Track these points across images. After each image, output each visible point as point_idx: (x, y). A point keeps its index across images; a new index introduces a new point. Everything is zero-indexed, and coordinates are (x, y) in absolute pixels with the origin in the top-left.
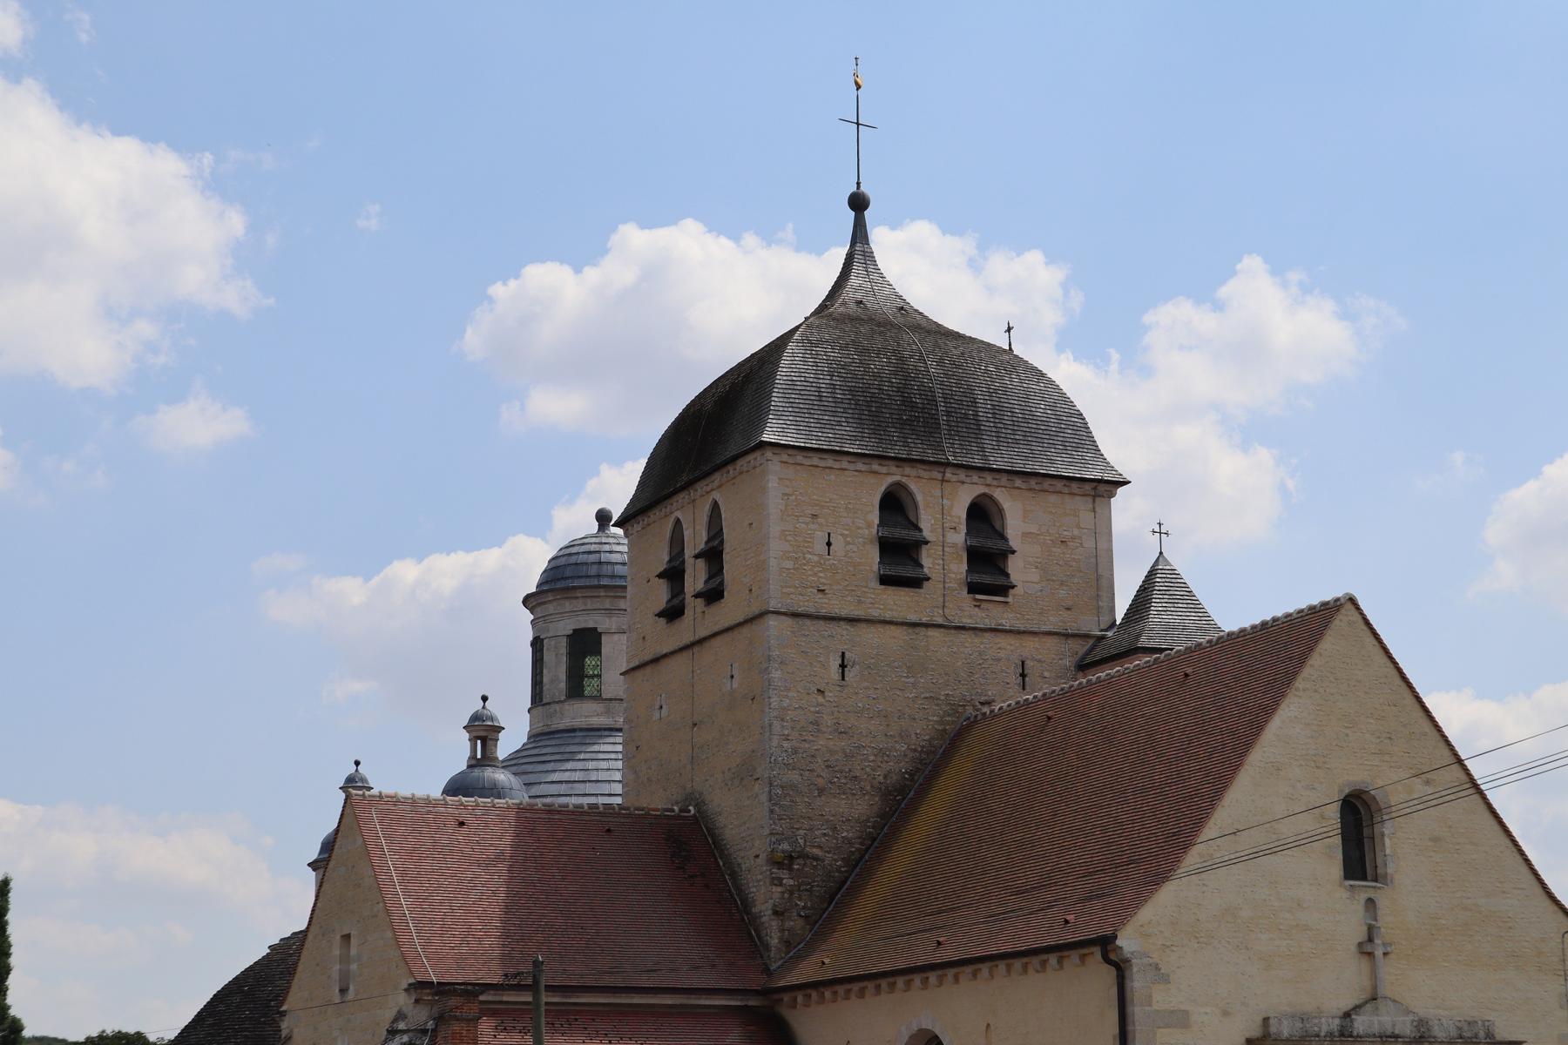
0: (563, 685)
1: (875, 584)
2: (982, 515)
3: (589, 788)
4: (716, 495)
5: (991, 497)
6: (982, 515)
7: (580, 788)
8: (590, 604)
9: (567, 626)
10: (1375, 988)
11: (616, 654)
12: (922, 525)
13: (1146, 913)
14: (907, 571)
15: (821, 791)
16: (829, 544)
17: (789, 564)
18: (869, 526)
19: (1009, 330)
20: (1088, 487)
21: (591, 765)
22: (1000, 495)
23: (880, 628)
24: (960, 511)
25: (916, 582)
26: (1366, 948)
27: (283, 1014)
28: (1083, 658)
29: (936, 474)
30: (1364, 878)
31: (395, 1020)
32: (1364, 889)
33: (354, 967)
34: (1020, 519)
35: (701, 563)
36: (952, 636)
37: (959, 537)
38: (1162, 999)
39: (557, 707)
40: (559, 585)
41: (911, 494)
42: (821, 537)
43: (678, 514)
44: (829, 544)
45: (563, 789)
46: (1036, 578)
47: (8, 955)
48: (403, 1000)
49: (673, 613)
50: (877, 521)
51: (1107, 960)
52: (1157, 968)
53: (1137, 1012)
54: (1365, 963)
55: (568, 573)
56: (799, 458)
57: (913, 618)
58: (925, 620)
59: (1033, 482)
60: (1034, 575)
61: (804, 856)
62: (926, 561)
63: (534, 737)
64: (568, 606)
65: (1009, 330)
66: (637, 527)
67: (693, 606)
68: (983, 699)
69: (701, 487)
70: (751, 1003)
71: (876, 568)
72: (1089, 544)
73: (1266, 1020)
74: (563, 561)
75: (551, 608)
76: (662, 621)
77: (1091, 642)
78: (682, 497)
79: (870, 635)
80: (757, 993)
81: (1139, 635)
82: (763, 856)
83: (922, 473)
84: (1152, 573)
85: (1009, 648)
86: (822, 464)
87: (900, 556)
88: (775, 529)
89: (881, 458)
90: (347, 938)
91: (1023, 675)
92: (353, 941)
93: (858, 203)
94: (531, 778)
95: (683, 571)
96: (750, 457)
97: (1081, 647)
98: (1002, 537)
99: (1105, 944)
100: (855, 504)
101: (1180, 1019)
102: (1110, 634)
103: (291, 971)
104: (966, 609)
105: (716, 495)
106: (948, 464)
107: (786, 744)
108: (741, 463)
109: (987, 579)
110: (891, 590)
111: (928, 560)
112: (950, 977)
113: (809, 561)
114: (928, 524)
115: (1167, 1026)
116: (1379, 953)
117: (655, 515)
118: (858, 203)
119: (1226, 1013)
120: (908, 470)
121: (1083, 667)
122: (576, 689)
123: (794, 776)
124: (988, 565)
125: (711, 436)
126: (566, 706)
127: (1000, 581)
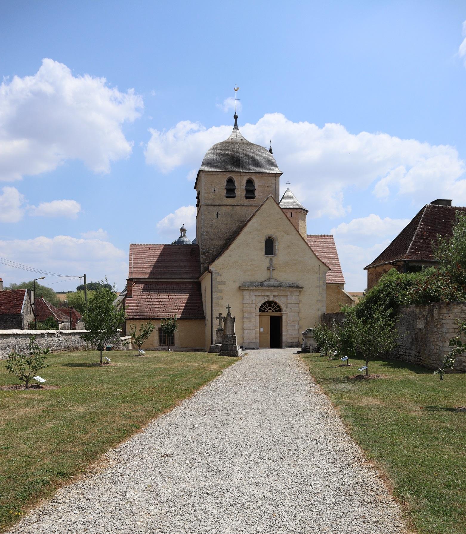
1: (225, 198)
2: (250, 182)
6: (250, 182)
22: (253, 178)
26: (269, 269)
32: (270, 257)
37: (244, 187)
38: (219, 279)
51: (209, 272)
54: (269, 271)
56: (208, 173)
61: (208, 252)
62: (236, 192)
72: (274, 187)
79: (223, 209)
87: (230, 192)
93: (236, 117)
98: (254, 186)
101: (224, 283)
104: (245, 202)
109: (250, 195)
110: (228, 199)
116: (271, 269)
118: (236, 117)
119: (234, 282)
123: (207, 237)
127: (253, 196)
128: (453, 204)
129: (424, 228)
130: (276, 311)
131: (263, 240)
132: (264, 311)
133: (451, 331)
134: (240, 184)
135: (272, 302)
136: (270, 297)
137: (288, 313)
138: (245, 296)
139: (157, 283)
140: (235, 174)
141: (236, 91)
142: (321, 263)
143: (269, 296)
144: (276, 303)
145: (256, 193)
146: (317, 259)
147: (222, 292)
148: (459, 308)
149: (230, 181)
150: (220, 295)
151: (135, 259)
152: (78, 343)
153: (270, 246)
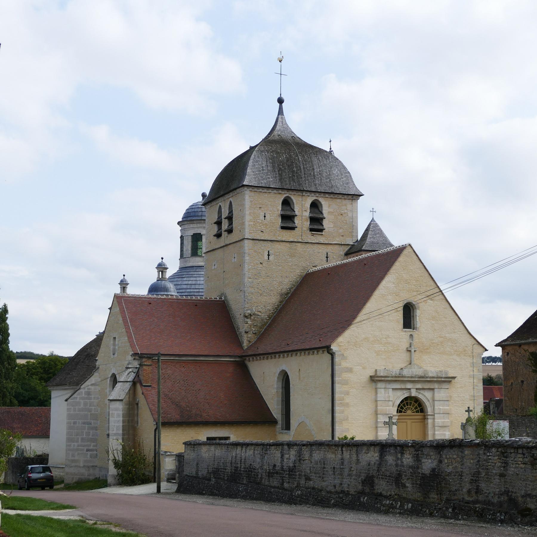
0: (190, 252)
2: (315, 205)
3: (197, 287)
4: (231, 199)
5: (318, 200)
6: (315, 205)
7: (193, 287)
8: (199, 225)
9: (191, 232)
10: (411, 361)
11: (204, 246)
12: (295, 210)
13: (340, 339)
14: (290, 225)
15: (261, 295)
16: (265, 217)
17: (252, 223)
18: (278, 211)
19: (330, 141)
20: (350, 197)
21: (198, 279)
22: (321, 200)
23: (281, 243)
24: (308, 205)
25: (293, 228)
27: (96, 360)
28: (347, 252)
29: (300, 193)
30: (411, 328)
31: (128, 364)
33: (117, 347)
34: (327, 207)
35: (226, 220)
36: (303, 246)
37: (307, 214)
38: (344, 364)
39: (188, 259)
40: (189, 219)
41: (292, 200)
42: (262, 214)
43: (220, 204)
44: (265, 217)
45: (189, 287)
46: (332, 226)
47: (8, 329)
48: (130, 358)
49: (218, 235)
50: (280, 209)
51: (328, 352)
52: (343, 355)
53: (337, 368)
54: (408, 353)
55: (192, 214)
57: (292, 240)
58: (295, 240)
59: (332, 196)
61: (254, 314)
63: (181, 269)
64: (192, 226)
65: (330, 141)
66: (208, 206)
67: (224, 234)
68: (314, 265)
69: (227, 196)
70: (237, 360)
71: (280, 224)
72: (350, 214)
73: (376, 370)
74: (190, 211)
75: (186, 226)
76: (216, 237)
77: (350, 246)
78: (221, 199)
79: (277, 246)
80: (239, 357)
81: (363, 246)
82: (242, 315)
83: (295, 193)
84: (369, 225)
85: (323, 250)
86: (263, 191)
87: (288, 220)
88: (247, 212)
89: (283, 189)
90: (115, 338)
91: (327, 257)
92: (117, 339)
93: (280, 101)
94: (178, 283)
95: (222, 222)
96: (241, 189)
97: (347, 248)
98: (322, 213)
99: (328, 349)
100: (274, 204)
101: (350, 370)
102: (356, 244)
103: (99, 346)
105: (231, 199)
106: (304, 191)
107: (249, 280)
108: (238, 190)
109: (316, 227)
110: (284, 231)
111: (297, 221)
112: (290, 355)
113: (258, 222)
114: (297, 210)
115: (346, 372)
116: (413, 351)
117: (214, 203)
118: (280, 101)
120: (291, 193)
121: (347, 254)
122: (195, 252)
124: (316, 222)
125: (230, 179)
126: (191, 259)
127: (320, 227)
131: (402, 304)
134: (302, 207)
136: (412, 390)
137: (436, 415)
138: (379, 390)
139: (179, 362)
141: (280, 61)
142: (475, 342)
143: (410, 389)
145: (325, 223)
153: (408, 313)
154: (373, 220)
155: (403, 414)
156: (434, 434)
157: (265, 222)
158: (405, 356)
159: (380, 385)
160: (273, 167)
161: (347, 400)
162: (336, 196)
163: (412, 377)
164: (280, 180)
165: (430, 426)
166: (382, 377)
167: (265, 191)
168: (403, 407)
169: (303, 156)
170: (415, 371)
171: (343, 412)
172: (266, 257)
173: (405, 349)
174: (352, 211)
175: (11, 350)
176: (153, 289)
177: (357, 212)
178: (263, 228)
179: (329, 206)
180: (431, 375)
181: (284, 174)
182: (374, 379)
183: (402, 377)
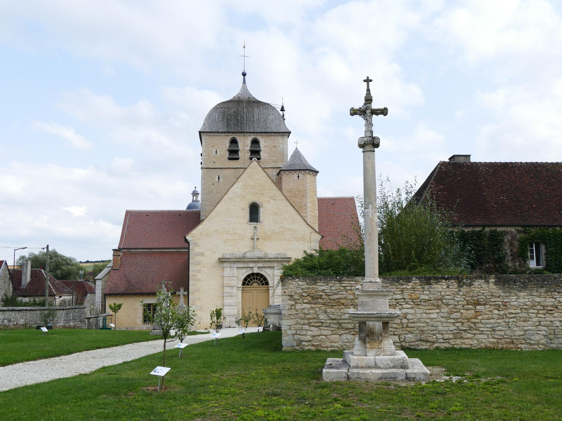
2: (255, 142)
6: (255, 142)
20: (281, 134)
22: (258, 138)
25: (238, 159)
32: (254, 224)
38: (197, 250)
54: (252, 240)
59: (267, 134)
60: (267, 155)
62: (240, 154)
72: (281, 146)
77: (266, 170)
79: (225, 171)
87: (233, 153)
89: (228, 132)
93: (244, 74)
101: (202, 254)
110: (231, 161)
116: (255, 239)
118: (244, 74)
124: (255, 153)
128: (472, 160)
129: (436, 187)
130: (263, 284)
132: (248, 284)
133: (287, 307)
134: (244, 144)
135: (258, 274)
139: (150, 253)
140: (238, 134)
142: (313, 230)
143: (252, 267)
144: (262, 276)
146: (307, 226)
147: (199, 264)
148: (294, 283)
149: (234, 142)
150: (198, 267)
151: (129, 226)
152: (9, 321)
153: (254, 211)
154: (296, 149)
155: (246, 286)
156: (274, 302)
157: (217, 156)
158: (249, 243)
159: (225, 265)
160: (223, 118)
161: (199, 276)
162: (270, 134)
163: (251, 258)
164: (227, 127)
165: (271, 295)
166: (228, 258)
167: (216, 134)
168: (248, 281)
169: (248, 109)
170: (257, 254)
171: (195, 285)
172: (217, 180)
173: (250, 238)
174: (283, 144)
175: (109, 256)
176: (189, 207)
177: (287, 144)
178: (215, 160)
179: (265, 141)
180: (271, 256)
181: (231, 122)
182: (222, 261)
183: (245, 258)
